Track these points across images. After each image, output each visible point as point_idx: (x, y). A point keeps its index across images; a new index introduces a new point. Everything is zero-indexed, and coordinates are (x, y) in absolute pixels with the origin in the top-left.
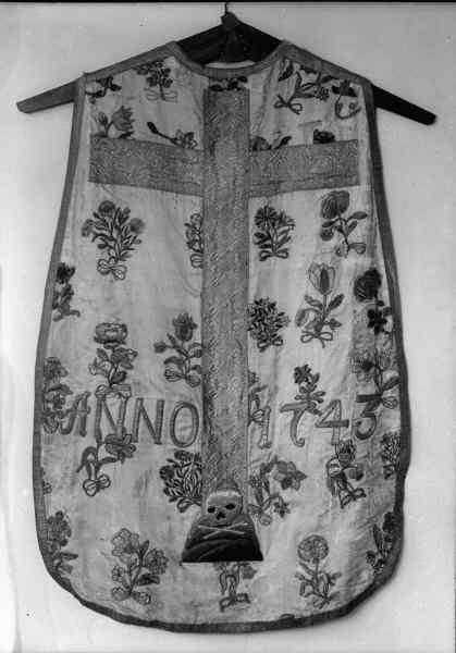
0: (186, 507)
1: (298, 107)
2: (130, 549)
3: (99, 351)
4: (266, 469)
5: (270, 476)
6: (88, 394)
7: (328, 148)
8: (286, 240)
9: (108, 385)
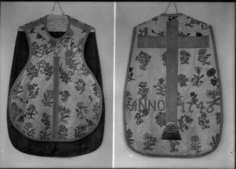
0: (162, 126)
1: (191, 26)
2: (148, 138)
3: (140, 89)
4: (182, 118)
5: (184, 119)
6: (136, 101)
7: (200, 37)
8: (188, 59)
9: (142, 97)
